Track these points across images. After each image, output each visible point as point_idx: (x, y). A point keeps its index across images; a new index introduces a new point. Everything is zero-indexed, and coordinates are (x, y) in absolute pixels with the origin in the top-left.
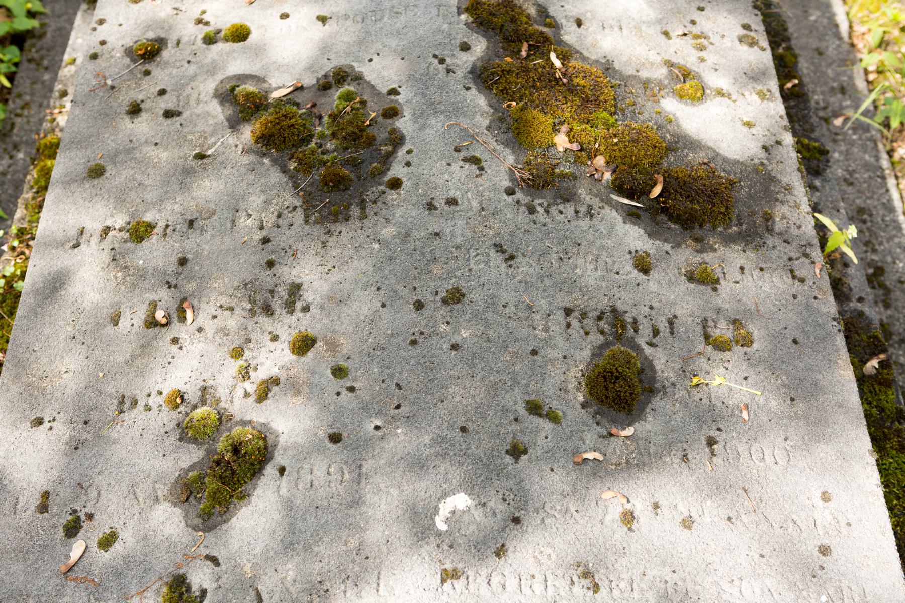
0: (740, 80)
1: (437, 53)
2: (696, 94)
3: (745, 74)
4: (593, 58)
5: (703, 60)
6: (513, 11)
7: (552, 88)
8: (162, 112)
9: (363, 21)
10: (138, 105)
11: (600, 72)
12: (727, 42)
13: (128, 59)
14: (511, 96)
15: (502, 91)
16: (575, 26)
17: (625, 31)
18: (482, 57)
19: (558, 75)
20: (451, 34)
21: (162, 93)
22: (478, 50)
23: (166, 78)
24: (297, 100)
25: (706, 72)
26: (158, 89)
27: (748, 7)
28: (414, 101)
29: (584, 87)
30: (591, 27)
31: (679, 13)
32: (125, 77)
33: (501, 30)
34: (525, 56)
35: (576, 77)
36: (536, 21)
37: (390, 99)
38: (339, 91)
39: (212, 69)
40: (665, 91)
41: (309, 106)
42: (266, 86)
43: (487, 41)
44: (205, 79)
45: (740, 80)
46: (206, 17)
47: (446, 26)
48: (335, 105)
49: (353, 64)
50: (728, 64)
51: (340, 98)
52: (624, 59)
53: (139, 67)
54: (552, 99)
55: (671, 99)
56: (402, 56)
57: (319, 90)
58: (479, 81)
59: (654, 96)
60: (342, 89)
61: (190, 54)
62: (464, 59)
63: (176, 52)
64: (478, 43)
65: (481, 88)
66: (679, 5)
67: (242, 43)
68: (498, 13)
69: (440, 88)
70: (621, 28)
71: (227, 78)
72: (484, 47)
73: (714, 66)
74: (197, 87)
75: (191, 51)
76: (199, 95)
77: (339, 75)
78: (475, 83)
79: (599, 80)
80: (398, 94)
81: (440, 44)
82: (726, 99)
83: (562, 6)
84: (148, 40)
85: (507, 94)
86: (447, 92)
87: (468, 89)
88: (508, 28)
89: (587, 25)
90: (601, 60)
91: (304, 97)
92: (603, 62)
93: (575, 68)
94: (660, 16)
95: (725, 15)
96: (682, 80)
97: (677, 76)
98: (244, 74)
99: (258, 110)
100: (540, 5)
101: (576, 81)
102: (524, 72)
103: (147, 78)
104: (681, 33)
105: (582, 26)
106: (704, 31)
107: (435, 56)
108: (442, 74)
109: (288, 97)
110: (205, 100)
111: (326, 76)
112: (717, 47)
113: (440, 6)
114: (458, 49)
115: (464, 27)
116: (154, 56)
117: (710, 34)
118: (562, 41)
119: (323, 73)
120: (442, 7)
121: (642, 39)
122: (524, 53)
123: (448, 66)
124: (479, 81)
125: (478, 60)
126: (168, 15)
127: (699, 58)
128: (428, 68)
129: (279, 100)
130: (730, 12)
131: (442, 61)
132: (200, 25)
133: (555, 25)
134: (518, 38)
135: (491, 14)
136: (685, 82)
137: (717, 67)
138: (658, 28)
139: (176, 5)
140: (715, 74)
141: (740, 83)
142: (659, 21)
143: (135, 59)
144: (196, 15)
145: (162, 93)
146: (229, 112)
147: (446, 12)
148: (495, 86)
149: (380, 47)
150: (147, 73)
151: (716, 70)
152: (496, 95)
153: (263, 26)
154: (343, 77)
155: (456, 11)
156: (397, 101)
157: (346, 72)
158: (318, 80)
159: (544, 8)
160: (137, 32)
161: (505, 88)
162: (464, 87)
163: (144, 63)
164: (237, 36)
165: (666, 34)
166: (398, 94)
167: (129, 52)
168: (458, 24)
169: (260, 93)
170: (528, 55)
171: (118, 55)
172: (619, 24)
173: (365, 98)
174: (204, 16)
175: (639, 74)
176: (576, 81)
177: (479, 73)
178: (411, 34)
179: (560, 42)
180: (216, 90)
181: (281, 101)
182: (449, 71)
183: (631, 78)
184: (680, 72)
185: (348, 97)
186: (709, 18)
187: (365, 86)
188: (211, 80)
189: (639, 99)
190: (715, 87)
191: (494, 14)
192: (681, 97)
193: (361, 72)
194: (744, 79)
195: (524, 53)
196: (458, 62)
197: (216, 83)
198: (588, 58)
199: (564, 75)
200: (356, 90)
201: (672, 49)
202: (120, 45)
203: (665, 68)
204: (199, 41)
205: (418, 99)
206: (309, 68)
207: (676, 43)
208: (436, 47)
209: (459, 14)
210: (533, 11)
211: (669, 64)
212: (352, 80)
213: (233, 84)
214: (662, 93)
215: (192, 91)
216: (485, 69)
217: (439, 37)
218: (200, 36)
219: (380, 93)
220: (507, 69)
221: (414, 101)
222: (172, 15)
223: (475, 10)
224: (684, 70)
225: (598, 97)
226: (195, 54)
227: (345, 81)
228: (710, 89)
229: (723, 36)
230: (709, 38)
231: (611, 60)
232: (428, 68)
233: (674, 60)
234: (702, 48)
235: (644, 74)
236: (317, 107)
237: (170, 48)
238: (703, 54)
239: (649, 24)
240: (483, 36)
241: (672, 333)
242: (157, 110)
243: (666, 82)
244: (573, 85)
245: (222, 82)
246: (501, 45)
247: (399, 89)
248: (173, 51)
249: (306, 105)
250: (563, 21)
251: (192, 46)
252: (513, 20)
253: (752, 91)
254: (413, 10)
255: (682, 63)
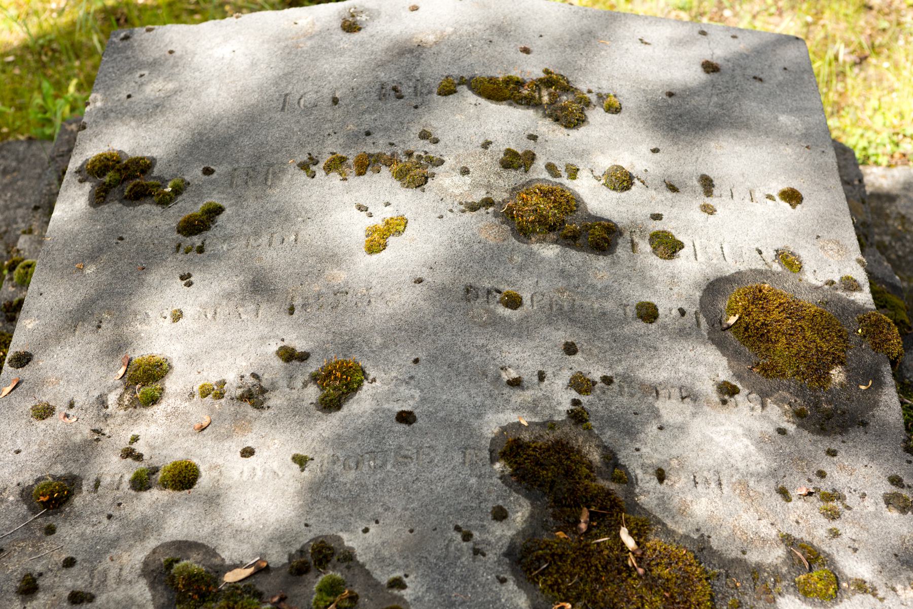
0: (889, 566)
1: (460, 524)
2: (828, 590)
3: (896, 555)
4: (681, 531)
5: (835, 534)
6: (568, 458)
7: (623, 581)
8: (67, 594)
9: (357, 467)
10: (34, 580)
11: (690, 556)
12: (869, 506)
13: (25, 506)
14: (564, 594)
15: (551, 586)
16: (656, 481)
17: (726, 489)
18: (524, 530)
19: (632, 561)
20: (480, 494)
21: (69, 563)
22: (519, 519)
23: (77, 541)
24: (259, 588)
25: (841, 553)
26: (64, 556)
27: (897, 449)
28: (427, 599)
29: (668, 580)
30: (679, 483)
31: (802, 459)
32: (19, 535)
33: (551, 488)
34: (584, 530)
35: (657, 564)
36: (600, 474)
37: (391, 594)
38: (320, 579)
39: (143, 528)
40: (784, 583)
41: (276, 599)
42: (216, 561)
43: (532, 504)
44: (131, 546)
45: (889, 566)
46: (139, 447)
47: (473, 480)
48: (313, 601)
49: (341, 534)
50: (871, 541)
51: (320, 590)
52: (725, 534)
53: (40, 520)
54: (622, 600)
55: (792, 597)
56: (410, 527)
57: (291, 573)
58: (519, 568)
59: (768, 591)
60: (324, 576)
61: (111, 505)
62: (498, 533)
63: (93, 499)
64: (518, 508)
65: (521, 579)
66: (801, 447)
67: (187, 491)
68: (546, 462)
69: (464, 579)
70: (720, 484)
71: (162, 546)
72: (527, 515)
73: (851, 544)
74: (120, 557)
75: (114, 501)
76: (121, 569)
77: (320, 552)
78: (514, 572)
79: (689, 569)
80: (404, 587)
81: (465, 509)
82: (870, 596)
83: (638, 450)
84: (53, 477)
85: (559, 590)
86: (474, 587)
87: (503, 581)
88: (562, 487)
89: (673, 478)
90: (692, 535)
91: (270, 583)
92: (695, 537)
93: (655, 550)
94: (774, 465)
95: (866, 463)
96: (807, 567)
97: (800, 561)
98: (187, 541)
99: (204, 601)
100: (605, 448)
101: (656, 571)
102: (584, 556)
103: (50, 538)
104: (804, 492)
105: (666, 481)
106: (837, 488)
107: (458, 529)
108: (466, 559)
109: (247, 583)
110: (129, 579)
111: (302, 552)
112: (856, 513)
113: (466, 448)
114: (490, 517)
115: (500, 481)
116: (61, 504)
117: (846, 493)
118: (638, 504)
119: (298, 547)
120: (468, 451)
121: (749, 501)
122: (583, 526)
123: (475, 544)
124: (519, 568)
125: (518, 534)
126: (86, 441)
127: (831, 530)
128: (447, 546)
129: (234, 586)
130: (872, 458)
131: (467, 537)
132: (129, 460)
133: (627, 480)
134: (575, 501)
135: (538, 463)
136: (811, 570)
137: (856, 546)
138: (772, 483)
139: (97, 427)
140: (854, 557)
141: (890, 571)
142: (773, 474)
143: (35, 507)
144: (124, 443)
145: (69, 563)
146: (162, 601)
147: (475, 458)
148: (542, 579)
149: (380, 510)
150: (50, 531)
151: (855, 550)
152: (543, 592)
153: (217, 466)
154: (326, 556)
155: (488, 456)
156: (401, 598)
157: (330, 548)
158: (291, 557)
159: (611, 452)
160: (40, 465)
161: (556, 581)
162: (498, 577)
163: (47, 514)
164: (180, 481)
165: (784, 493)
166: (404, 587)
167: (26, 494)
168: (491, 477)
169: (207, 572)
170: (590, 528)
171: (11, 498)
172: (716, 478)
173: (356, 591)
174: (135, 446)
175: (746, 556)
176: (656, 571)
177: (519, 556)
178: (424, 492)
179: (634, 507)
180: (146, 564)
181: (237, 588)
182: (476, 552)
183: (735, 564)
184: (803, 554)
185: (332, 588)
186: (843, 468)
187: (356, 571)
188: (139, 548)
189: (747, 598)
190: (854, 577)
191: (542, 464)
192: (806, 594)
193: (353, 549)
194: (894, 564)
195: (583, 526)
196: (490, 538)
197: (146, 553)
198: (674, 531)
199: (639, 560)
200: (344, 578)
201: (793, 517)
202: (15, 483)
203: (783, 546)
204: (126, 485)
205: (432, 597)
206: (280, 538)
207: (798, 507)
208: (459, 513)
209: (493, 461)
210: (595, 457)
211: (788, 540)
212: (339, 560)
213: (171, 554)
214: (780, 587)
215: (111, 564)
216: (527, 550)
217: (464, 498)
218: (128, 477)
219: (377, 584)
220: (559, 551)
221: (427, 599)
222: (91, 441)
223: (515, 457)
224: (810, 552)
225: (688, 596)
226: (119, 504)
227: (328, 561)
228: (848, 580)
229: (863, 496)
230: (844, 498)
231: (706, 534)
232: (447, 546)
233: (796, 534)
234: (834, 515)
235: (753, 557)
236: (287, 601)
237: (84, 493)
238: (836, 524)
239: (759, 477)
240: (527, 496)
241: (755, 78)
242: (61, 590)
243: (784, 570)
244: (653, 578)
245: (154, 552)
246: (551, 510)
247: (405, 579)
248: (88, 498)
249: (273, 597)
250: (639, 473)
251: (116, 492)
252: (569, 473)
253: (907, 583)
254: (429, 454)
255: (807, 538)
